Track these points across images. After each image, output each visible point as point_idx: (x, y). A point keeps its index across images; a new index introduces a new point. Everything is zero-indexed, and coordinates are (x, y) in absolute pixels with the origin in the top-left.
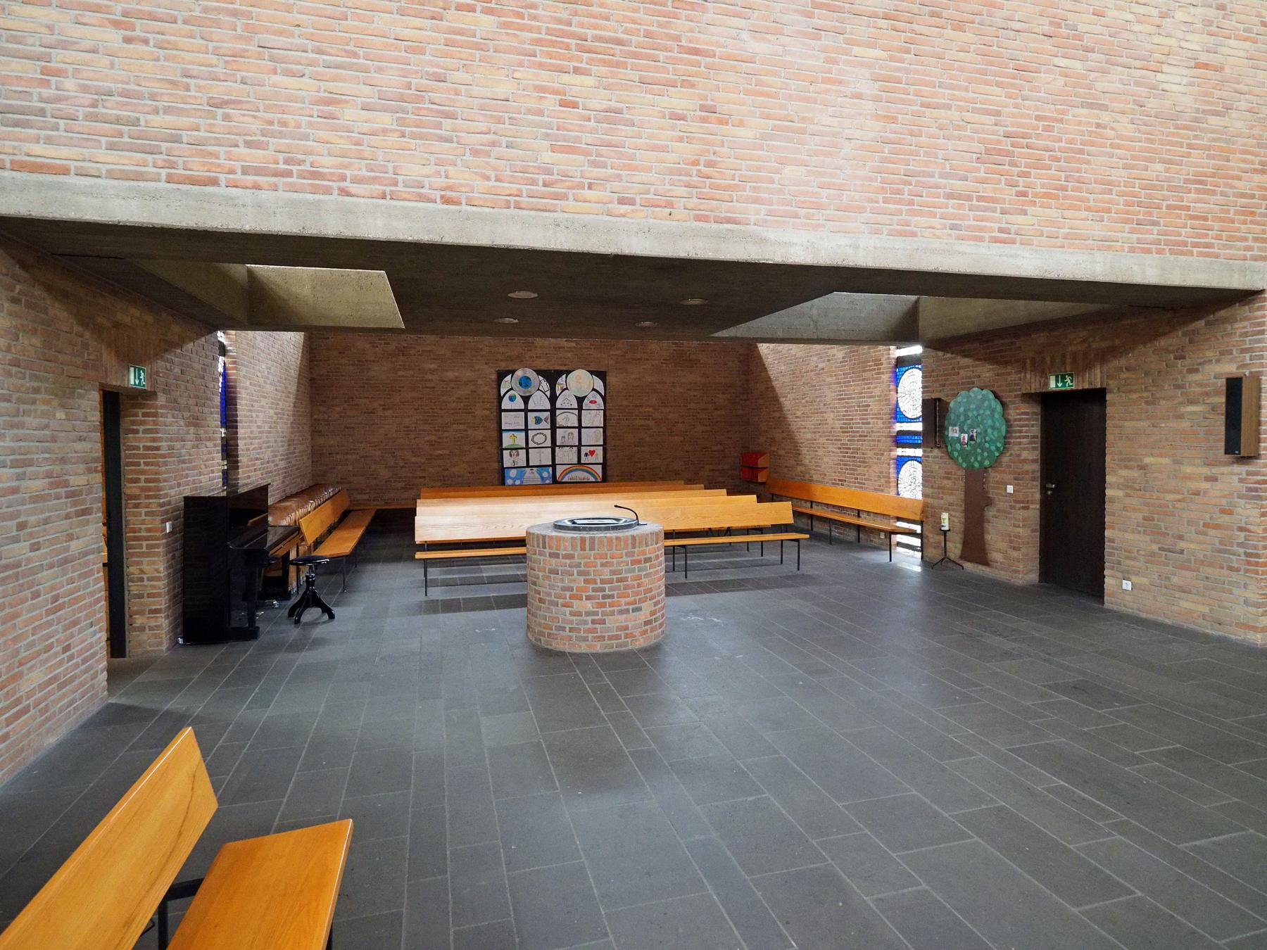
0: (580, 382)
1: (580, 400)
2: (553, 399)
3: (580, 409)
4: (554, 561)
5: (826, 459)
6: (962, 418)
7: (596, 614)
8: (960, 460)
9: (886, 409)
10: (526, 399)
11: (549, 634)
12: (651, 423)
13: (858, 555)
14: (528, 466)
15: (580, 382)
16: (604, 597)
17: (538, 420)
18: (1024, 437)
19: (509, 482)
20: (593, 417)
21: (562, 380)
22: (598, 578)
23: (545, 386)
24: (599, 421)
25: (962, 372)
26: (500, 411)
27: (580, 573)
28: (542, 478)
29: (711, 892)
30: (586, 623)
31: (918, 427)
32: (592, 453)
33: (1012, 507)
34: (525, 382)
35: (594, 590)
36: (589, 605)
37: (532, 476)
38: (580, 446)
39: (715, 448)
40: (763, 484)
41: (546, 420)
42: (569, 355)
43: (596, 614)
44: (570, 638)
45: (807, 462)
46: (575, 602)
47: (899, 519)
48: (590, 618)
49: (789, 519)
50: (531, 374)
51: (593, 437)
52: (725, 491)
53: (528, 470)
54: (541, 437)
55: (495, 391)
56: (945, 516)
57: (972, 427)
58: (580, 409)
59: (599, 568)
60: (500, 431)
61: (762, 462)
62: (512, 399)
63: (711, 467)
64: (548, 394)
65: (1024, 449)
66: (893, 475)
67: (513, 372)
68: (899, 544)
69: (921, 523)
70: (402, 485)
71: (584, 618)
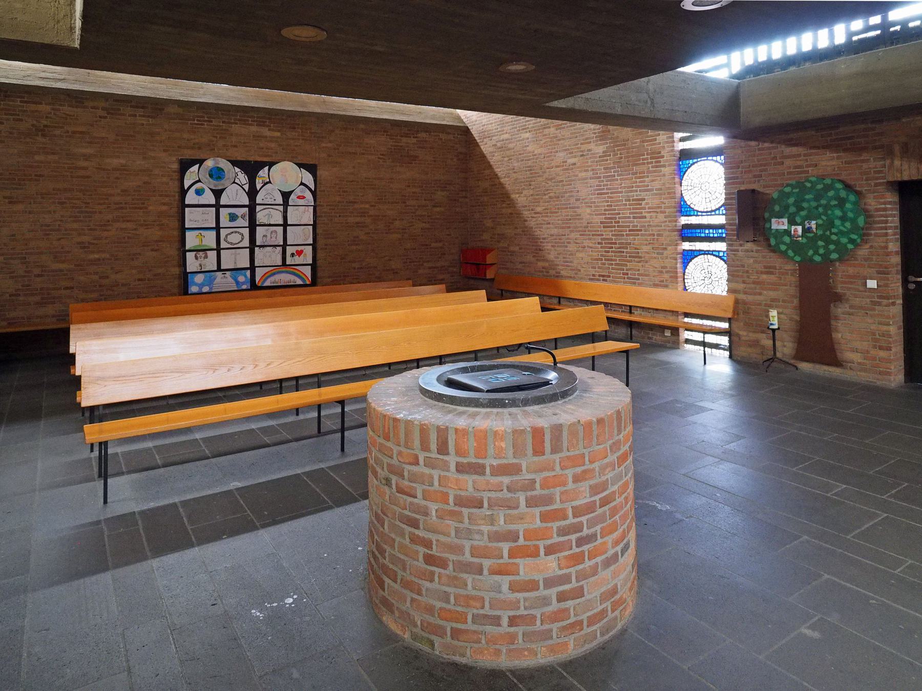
0: (285, 175)
1: (286, 195)
2: (252, 193)
3: (286, 204)
4: (469, 480)
5: (580, 255)
6: (792, 209)
7: (566, 579)
8: (791, 253)
9: (672, 203)
10: (218, 193)
11: (456, 633)
12: (368, 220)
13: (651, 356)
14: (219, 269)
15: (285, 175)
16: (580, 542)
17: (233, 218)
18: (890, 228)
19: (194, 289)
20: (302, 214)
21: (263, 173)
22: (568, 506)
23: (243, 178)
24: (308, 217)
25: (788, 162)
26: (183, 206)
27: (532, 503)
28: (237, 283)
29: (204, 448)
30: (546, 601)
31: (720, 220)
32: (299, 253)
33: (874, 303)
34: (216, 173)
35: (563, 532)
36: (551, 565)
37: (223, 282)
38: (284, 246)
39: (433, 245)
40: (493, 280)
41: (243, 217)
42: (273, 145)
43: (566, 579)
44: (512, 638)
45: (551, 257)
46: (523, 564)
47: (687, 315)
48: (553, 592)
49: (603, 326)
50: (224, 164)
51: (300, 236)
52: (443, 287)
53: (219, 274)
54: (238, 236)
55: (177, 183)
56: (774, 313)
57: (809, 218)
58: (286, 204)
59: (571, 486)
60: (183, 230)
61: (490, 259)
62: (199, 192)
63: (430, 265)
64: (246, 187)
65: (891, 241)
66: (680, 270)
67: (201, 162)
68: (688, 341)
69: (729, 320)
70: (37, 298)
71: (542, 592)
